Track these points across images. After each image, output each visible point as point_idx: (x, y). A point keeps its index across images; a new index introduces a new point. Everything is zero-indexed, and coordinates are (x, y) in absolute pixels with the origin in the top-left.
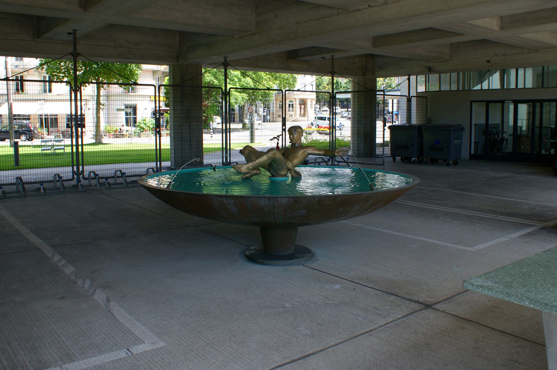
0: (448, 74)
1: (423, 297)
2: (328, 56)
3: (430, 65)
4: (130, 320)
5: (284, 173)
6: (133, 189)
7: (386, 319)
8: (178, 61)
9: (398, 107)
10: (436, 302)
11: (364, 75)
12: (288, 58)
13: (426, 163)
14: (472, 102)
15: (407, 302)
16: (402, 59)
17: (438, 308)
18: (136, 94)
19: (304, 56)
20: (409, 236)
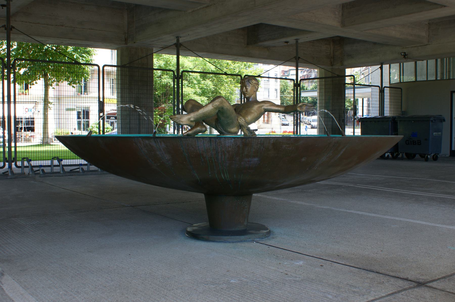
0: (425, 61)
1: (412, 274)
2: (291, 40)
3: (405, 50)
4: (22, 295)
5: (234, 130)
6: (69, 177)
7: (365, 297)
8: (126, 43)
9: (369, 110)
10: (431, 279)
11: (332, 65)
12: (248, 44)
13: (402, 159)
14: (452, 92)
15: (392, 280)
16: (375, 43)
17: (434, 286)
18: (89, 96)
19: (265, 40)
20: (389, 217)
